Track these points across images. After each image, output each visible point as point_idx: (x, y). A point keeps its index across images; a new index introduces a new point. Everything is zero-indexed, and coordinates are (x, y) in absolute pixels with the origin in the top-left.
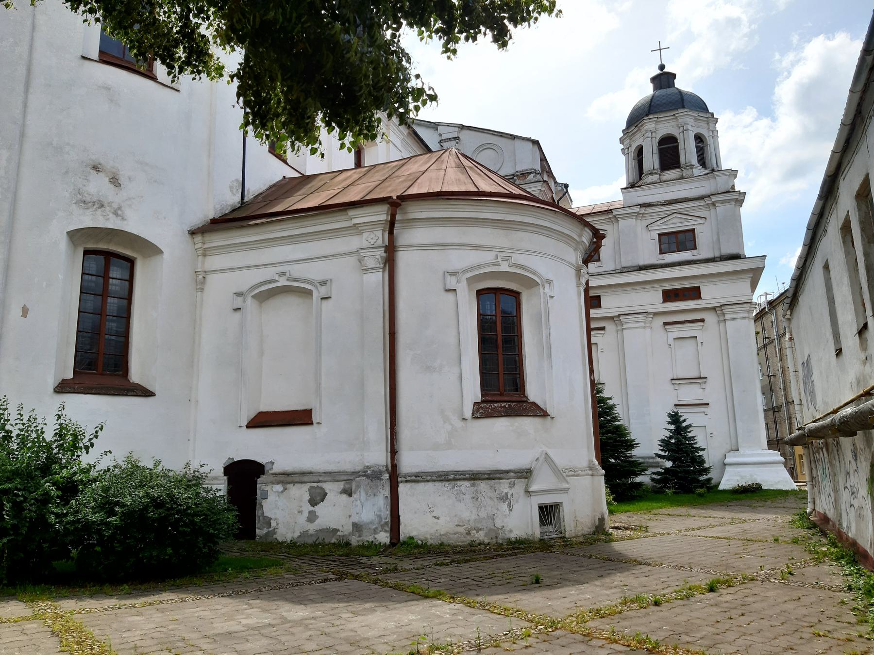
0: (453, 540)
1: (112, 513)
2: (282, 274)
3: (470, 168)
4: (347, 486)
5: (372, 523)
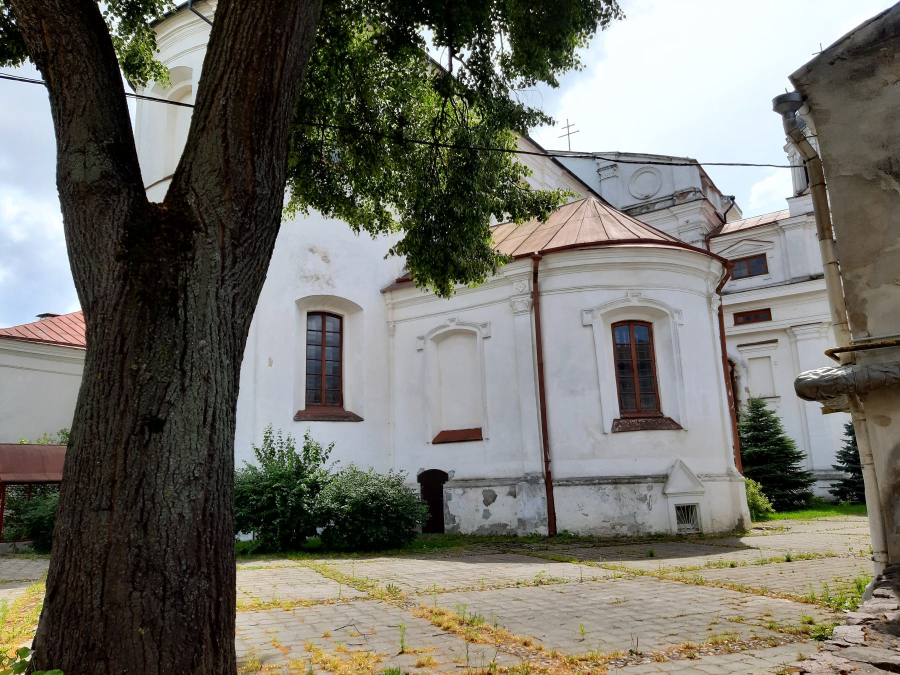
0: (601, 533)
1: (343, 503)
2: (452, 320)
3: (605, 216)
4: (512, 489)
5: (533, 519)
